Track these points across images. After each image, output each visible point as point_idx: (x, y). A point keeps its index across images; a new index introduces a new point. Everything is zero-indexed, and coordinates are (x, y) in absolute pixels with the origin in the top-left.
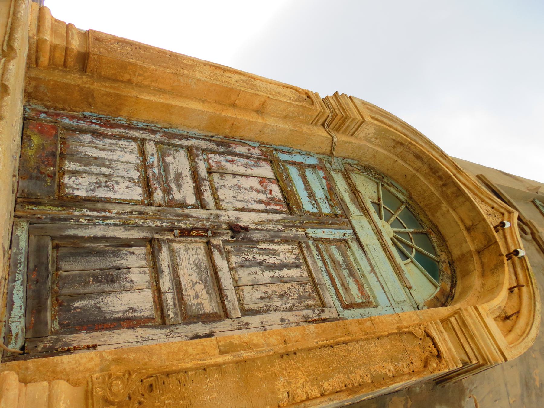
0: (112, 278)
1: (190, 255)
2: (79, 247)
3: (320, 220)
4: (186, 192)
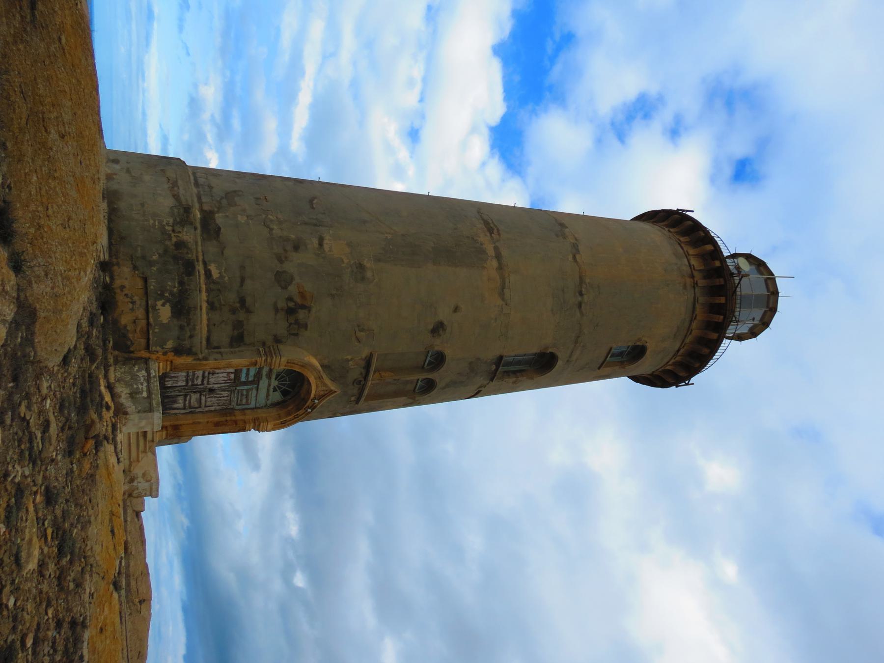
0: (175, 402)
1: (194, 397)
2: (168, 397)
3: (245, 383)
4: (199, 382)
